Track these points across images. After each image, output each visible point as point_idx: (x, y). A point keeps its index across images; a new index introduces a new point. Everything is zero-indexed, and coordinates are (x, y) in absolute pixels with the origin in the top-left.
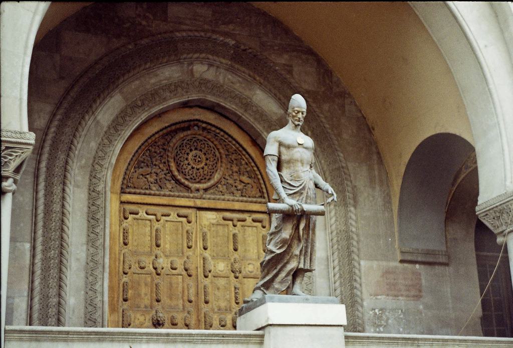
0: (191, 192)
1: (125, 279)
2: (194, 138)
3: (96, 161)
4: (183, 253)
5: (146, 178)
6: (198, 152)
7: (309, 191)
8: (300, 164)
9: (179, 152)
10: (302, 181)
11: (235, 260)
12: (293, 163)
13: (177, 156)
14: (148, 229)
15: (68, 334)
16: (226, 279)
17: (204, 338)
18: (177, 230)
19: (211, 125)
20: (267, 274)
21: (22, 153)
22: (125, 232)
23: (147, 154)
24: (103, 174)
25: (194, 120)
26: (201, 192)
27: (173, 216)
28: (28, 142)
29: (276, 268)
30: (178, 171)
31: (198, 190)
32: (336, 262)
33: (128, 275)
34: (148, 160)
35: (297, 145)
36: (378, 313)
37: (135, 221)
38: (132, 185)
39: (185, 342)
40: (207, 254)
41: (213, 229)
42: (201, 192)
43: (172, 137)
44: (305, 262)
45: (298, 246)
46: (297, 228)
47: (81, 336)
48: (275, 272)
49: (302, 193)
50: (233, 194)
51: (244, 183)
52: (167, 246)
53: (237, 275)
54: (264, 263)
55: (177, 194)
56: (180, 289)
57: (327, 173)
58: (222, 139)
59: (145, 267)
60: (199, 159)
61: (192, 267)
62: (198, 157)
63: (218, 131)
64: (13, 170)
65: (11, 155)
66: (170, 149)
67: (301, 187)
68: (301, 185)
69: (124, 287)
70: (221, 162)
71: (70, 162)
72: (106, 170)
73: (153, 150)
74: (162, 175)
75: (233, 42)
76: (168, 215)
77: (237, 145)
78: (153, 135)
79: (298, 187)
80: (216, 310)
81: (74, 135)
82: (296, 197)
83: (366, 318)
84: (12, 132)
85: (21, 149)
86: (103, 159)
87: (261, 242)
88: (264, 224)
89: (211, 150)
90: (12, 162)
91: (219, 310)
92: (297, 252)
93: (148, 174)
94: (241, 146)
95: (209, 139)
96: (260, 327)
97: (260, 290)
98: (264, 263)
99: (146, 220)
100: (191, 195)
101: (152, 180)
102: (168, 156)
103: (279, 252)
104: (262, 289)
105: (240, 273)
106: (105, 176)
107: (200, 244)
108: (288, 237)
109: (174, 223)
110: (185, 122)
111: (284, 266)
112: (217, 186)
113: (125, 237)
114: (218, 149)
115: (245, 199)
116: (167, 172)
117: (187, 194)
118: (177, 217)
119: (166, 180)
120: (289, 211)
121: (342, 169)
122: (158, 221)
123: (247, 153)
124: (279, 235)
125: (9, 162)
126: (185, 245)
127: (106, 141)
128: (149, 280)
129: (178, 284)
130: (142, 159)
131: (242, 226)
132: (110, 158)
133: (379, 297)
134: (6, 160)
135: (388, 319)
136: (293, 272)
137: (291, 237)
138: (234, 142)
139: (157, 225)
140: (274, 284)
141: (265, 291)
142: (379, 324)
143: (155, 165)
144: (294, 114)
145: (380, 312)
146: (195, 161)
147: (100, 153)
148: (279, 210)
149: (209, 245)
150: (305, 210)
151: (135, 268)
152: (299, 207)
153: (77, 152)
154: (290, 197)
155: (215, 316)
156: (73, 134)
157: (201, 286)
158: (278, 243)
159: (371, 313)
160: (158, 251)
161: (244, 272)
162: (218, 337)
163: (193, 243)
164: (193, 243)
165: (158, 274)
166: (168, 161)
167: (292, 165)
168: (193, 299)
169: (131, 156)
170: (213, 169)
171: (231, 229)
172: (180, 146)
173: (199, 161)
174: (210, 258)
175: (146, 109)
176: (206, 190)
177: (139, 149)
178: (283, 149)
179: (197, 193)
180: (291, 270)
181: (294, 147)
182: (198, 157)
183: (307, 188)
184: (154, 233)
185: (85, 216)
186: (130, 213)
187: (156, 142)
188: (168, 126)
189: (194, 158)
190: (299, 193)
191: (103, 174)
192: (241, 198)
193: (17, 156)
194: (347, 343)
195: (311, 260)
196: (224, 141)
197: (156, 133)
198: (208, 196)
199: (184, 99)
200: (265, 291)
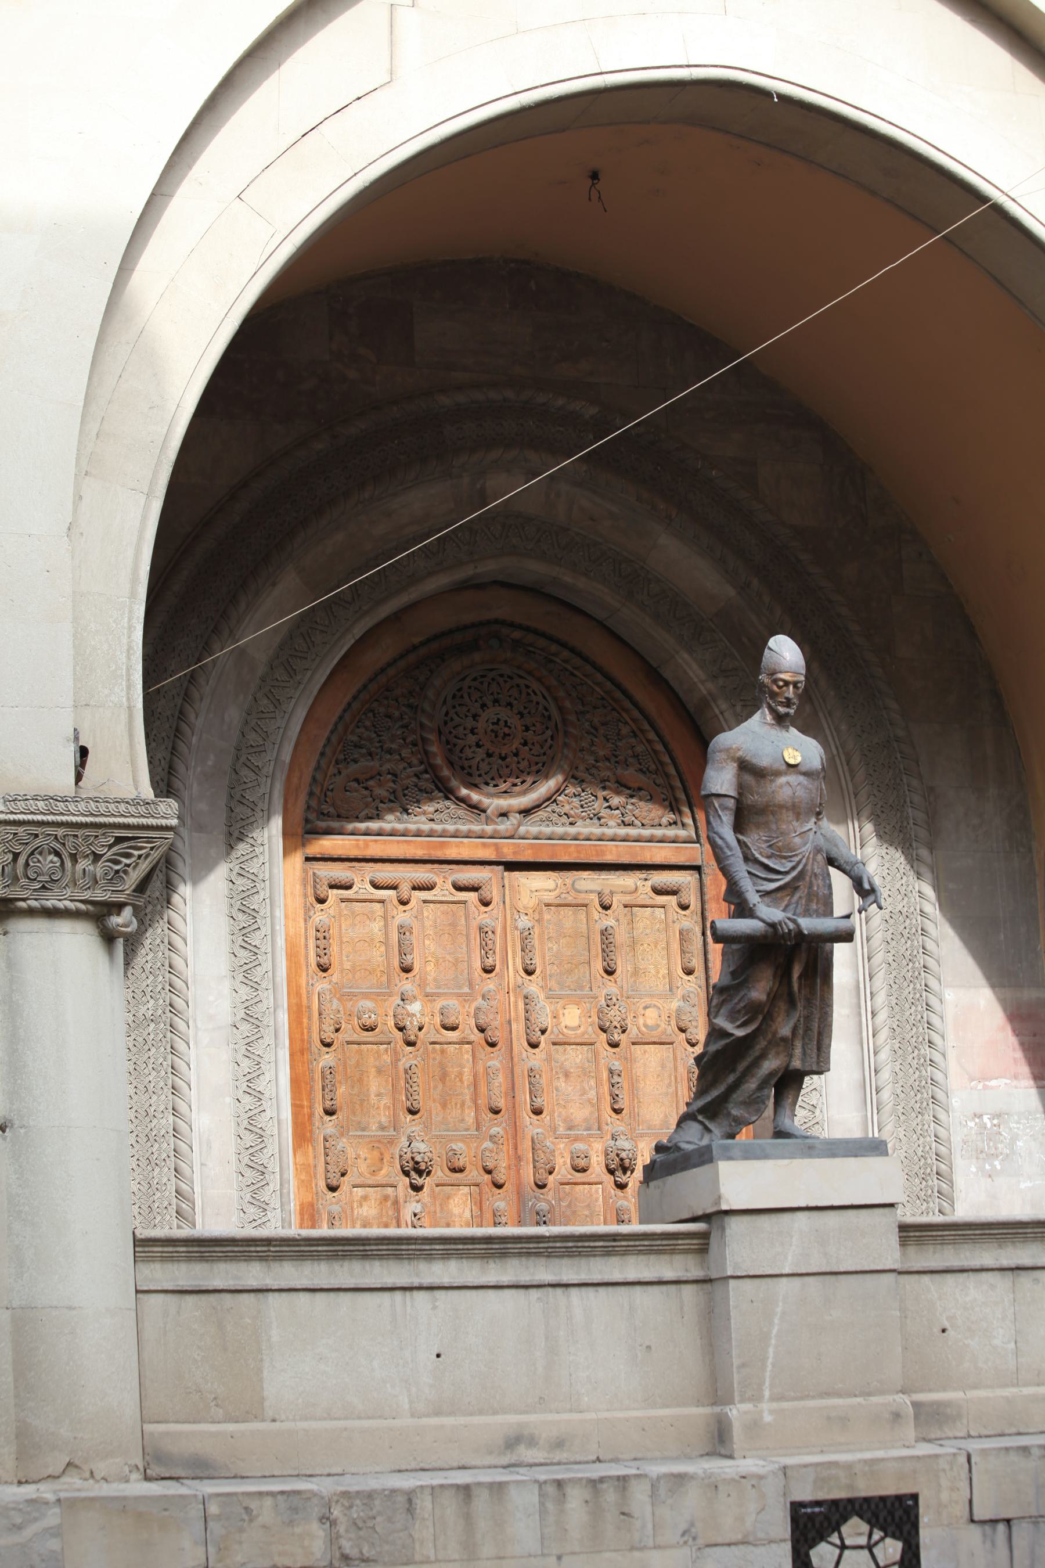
0: (488, 821)
1: (327, 1059)
2: (491, 670)
3: (243, 759)
4: (471, 986)
5: (366, 788)
6: (504, 713)
7: (814, 881)
8: (791, 815)
9: (452, 713)
10: (797, 859)
11: (609, 998)
12: (773, 813)
13: (446, 723)
14: (377, 926)
15: (269, 1245)
16: (585, 1048)
17: (570, 1244)
18: (454, 925)
19: (536, 632)
20: (713, 1084)
21: (152, 849)
22: (322, 935)
23: (368, 723)
24: (262, 791)
25: (489, 622)
26: (515, 818)
27: (443, 891)
28: (163, 822)
29: (734, 1070)
30: (451, 764)
31: (504, 815)
32: (881, 999)
33: (333, 1048)
34: (370, 740)
35: (784, 767)
36: (989, 1125)
37: (344, 904)
38: (332, 810)
39: (529, 1254)
40: (533, 986)
41: (547, 917)
42: (515, 818)
43: (432, 671)
44: (804, 1053)
45: (788, 1014)
46: (786, 974)
47: (297, 1249)
48: (731, 1079)
49: (797, 888)
50: (599, 819)
51: (629, 788)
52: (428, 968)
53: (616, 1037)
54: (705, 1059)
55: (451, 828)
56: (468, 1077)
57: (856, 758)
58: (567, 670)
59: (376, 1027)
60: (506, 730)
61: (495, 1022)
62: (502, 723)
63: (554, 648)
64: (133, 887)
65: (128, 856)
66: (427, 706)
67: (794, 874)
68: (793, 868)
69: (323, 1078)
70: (566, 733)
71: (181, 768)
72: (269, 780)
73: (382, 710)
74: (409, 777)
75: (593, 410)
76: (429, 887)
77: (608, 684)
78: (383, 670)
79: (787, 873)
80: (561, 1130)
81: (186, 694)
82: (782, 898)
83: (956, 1139)
84: (127, 803)
85: (149, 840)
86: (261, 751)
87: (676, 946)
88: (685, 901)
89: (538, 703)
90: (130, 869)
91: (570, 1128)
92: (785, 1031)
93: (372, 778)
94: (618, 686)
95: (529, 673)
96: (700, 1213)
97: (695, 1119)
98: (705, 1059)
99: (371, 901)
100: (489, 829)
101: (380, 792)
102: (422, 725)
103: (740, 1033)
104: (700, 1118)
105: (624, 1031)
106: (267, 796)
107: (515, 962)
108: (763, 997)
109: (445, 906)
110: (466, 627)
111: (756, 1063)
112: (555, 801)
113: (322, 951)
114: (556, 699)
115: (633, 832)
116: (422, 767)
117: (476, 828)
118: (453, 891)
119: (420, 790)
120: (764, 936)
121: (895, 744)
122: (404, 903)
123: (636, 705)
124: (742, 994)
125: (125, 872)
126: (477, 965)
127: (265, 701)
128: (387, 1058)
129: (462, 1066)
130: (355, 738)
131: (626, 906)
132: (277, 746)
133: (993, 1083)
134: (117, 867)
135: (1014, 1139)
136: (776, 1079)
137: (772, 995)
138: (599, 677)
139: (401, 916)
140: (730, 1105)
141: (707, 1123)
142: (993, 1151)
143: (390, 752)
144: (775, 688)
145: (995, 1122)
146: (496, 736)
147: (253, 738)
148: (741, 937)
149: (537, 961)
150: (806, 932)
151: (350, 1032)
152: (791, 926)
153: (194, 740)
154: (766, 899)
155: (562, 1146)
156: (183, 692)
157: (521, 1070)
158: (739, 1011)
159: (971, 1124)
160: (407, 985)
161: (633, 1032)
162: (604, 1241)
163: (498, 957)
164: (498, 957)
165: (410, 1044)
166: (424, 740)
167: (771, 817)
168: (501, 1103)
169: (327, 734)
170: (544, 754)
171: (596, 915)
172: (454, 697)
173: (505, 735)
174: (542, 996)
175: (365, 608)
176: (526, 812)
177: (345, 711)
178: (749, 779)
179: (502, 822)
180: (771, 1074)
181: (778, 774)
182: (502, 723)
183: (809, 874)
184: (394, 936)
185: (225, 908)
186: (332, 887)
187: (387, 690)
188: (422, 644)
189: (491, 727)
190: (790, 888)
191: (262, 791)
192: (623, 831)
193: (140, 857)
194: (904, 1242)
195: (819, 1049)
196: (572, 674)
197: (389, 665)
198: (534, 830)
199: (466, 572)
200: (707, 1123)
